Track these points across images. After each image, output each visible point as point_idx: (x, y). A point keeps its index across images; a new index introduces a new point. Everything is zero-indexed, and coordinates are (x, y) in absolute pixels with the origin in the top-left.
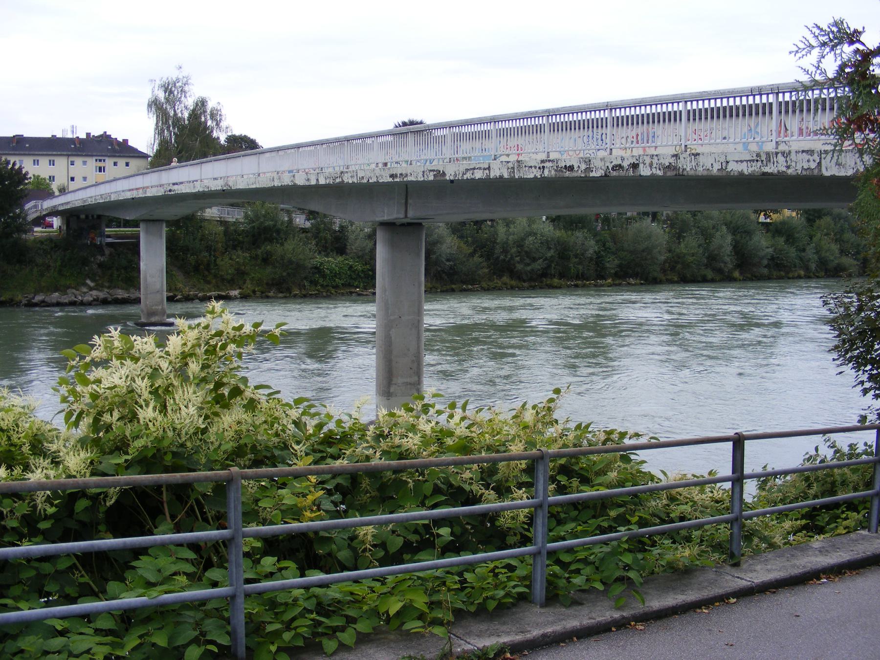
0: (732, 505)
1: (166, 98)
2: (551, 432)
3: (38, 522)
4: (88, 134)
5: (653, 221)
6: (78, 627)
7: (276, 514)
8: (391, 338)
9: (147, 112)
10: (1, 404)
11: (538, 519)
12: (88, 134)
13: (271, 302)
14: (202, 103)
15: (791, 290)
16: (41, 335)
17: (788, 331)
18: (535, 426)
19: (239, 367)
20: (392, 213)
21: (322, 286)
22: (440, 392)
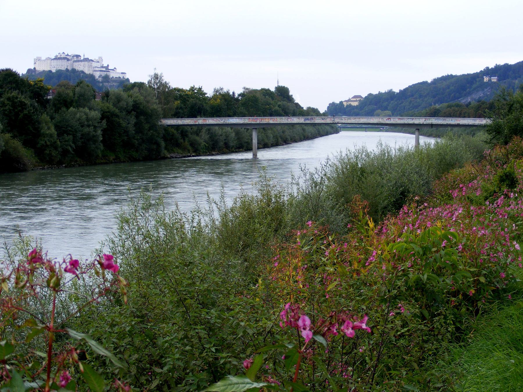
0: (81, 61)
1: (16, 90)
2: (126, 209)
3: (158, 118)
4: (292, 95)
5: (68, 108)
6: (78, 351)
7: (290, 315)
8: (402, 235)
9: (248, 87)
10: (1, 358)
11: (471, 120)
12: (292, 95)
13: (127, 172)
14: (166, 82)
15: (164, 172)
16: (177, 163)
17: (134, 196)
18: (44, 380)
19: (503, 308)
20: (262, 127)
21: (56, 148)
22: (68, 57)
